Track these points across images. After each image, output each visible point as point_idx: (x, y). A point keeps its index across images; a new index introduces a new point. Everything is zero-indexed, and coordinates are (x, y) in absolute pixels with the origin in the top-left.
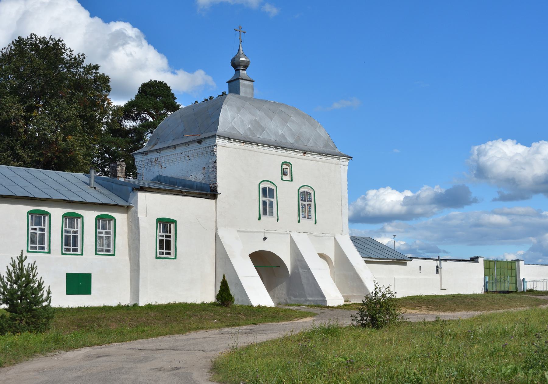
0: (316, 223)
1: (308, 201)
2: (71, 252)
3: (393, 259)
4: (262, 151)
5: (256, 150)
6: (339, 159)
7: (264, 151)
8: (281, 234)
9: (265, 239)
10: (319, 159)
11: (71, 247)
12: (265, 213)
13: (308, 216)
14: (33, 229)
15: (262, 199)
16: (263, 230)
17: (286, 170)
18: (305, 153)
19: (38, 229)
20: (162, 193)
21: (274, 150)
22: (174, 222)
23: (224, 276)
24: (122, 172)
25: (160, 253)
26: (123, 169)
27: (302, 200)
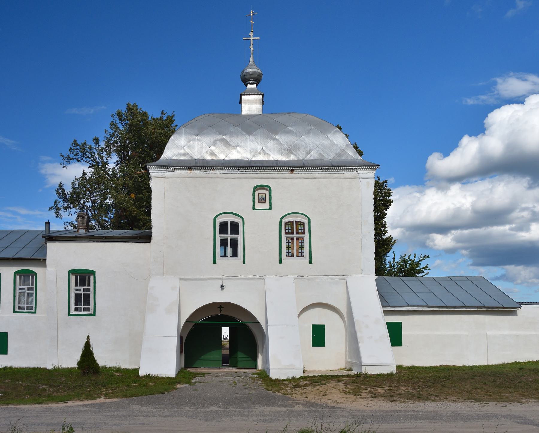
0: (311, 262)
1: (297, 233)
2: (26, 311)
3: (477, 307)
4: (220, 175)
5: (210, 175)
6: (356, 170)
7: (224, 176)
8: (250, 279)
9: (222, 286)
10: (319, 176)
11: (82, 307)
12: (290, 255)
13: (298, 252)
14: (20, 289)
15: (219, 237)
16: (221, 277)
17: (262, 196)
18: (293, 170)
19: (82, 290)
20: (84, 241)
21: (240, 172)
22: (93, 273)
23: (88, 338)
24: (83, 223)
25: (76, 310)
26: (83, 219)
27: (286, 233)
